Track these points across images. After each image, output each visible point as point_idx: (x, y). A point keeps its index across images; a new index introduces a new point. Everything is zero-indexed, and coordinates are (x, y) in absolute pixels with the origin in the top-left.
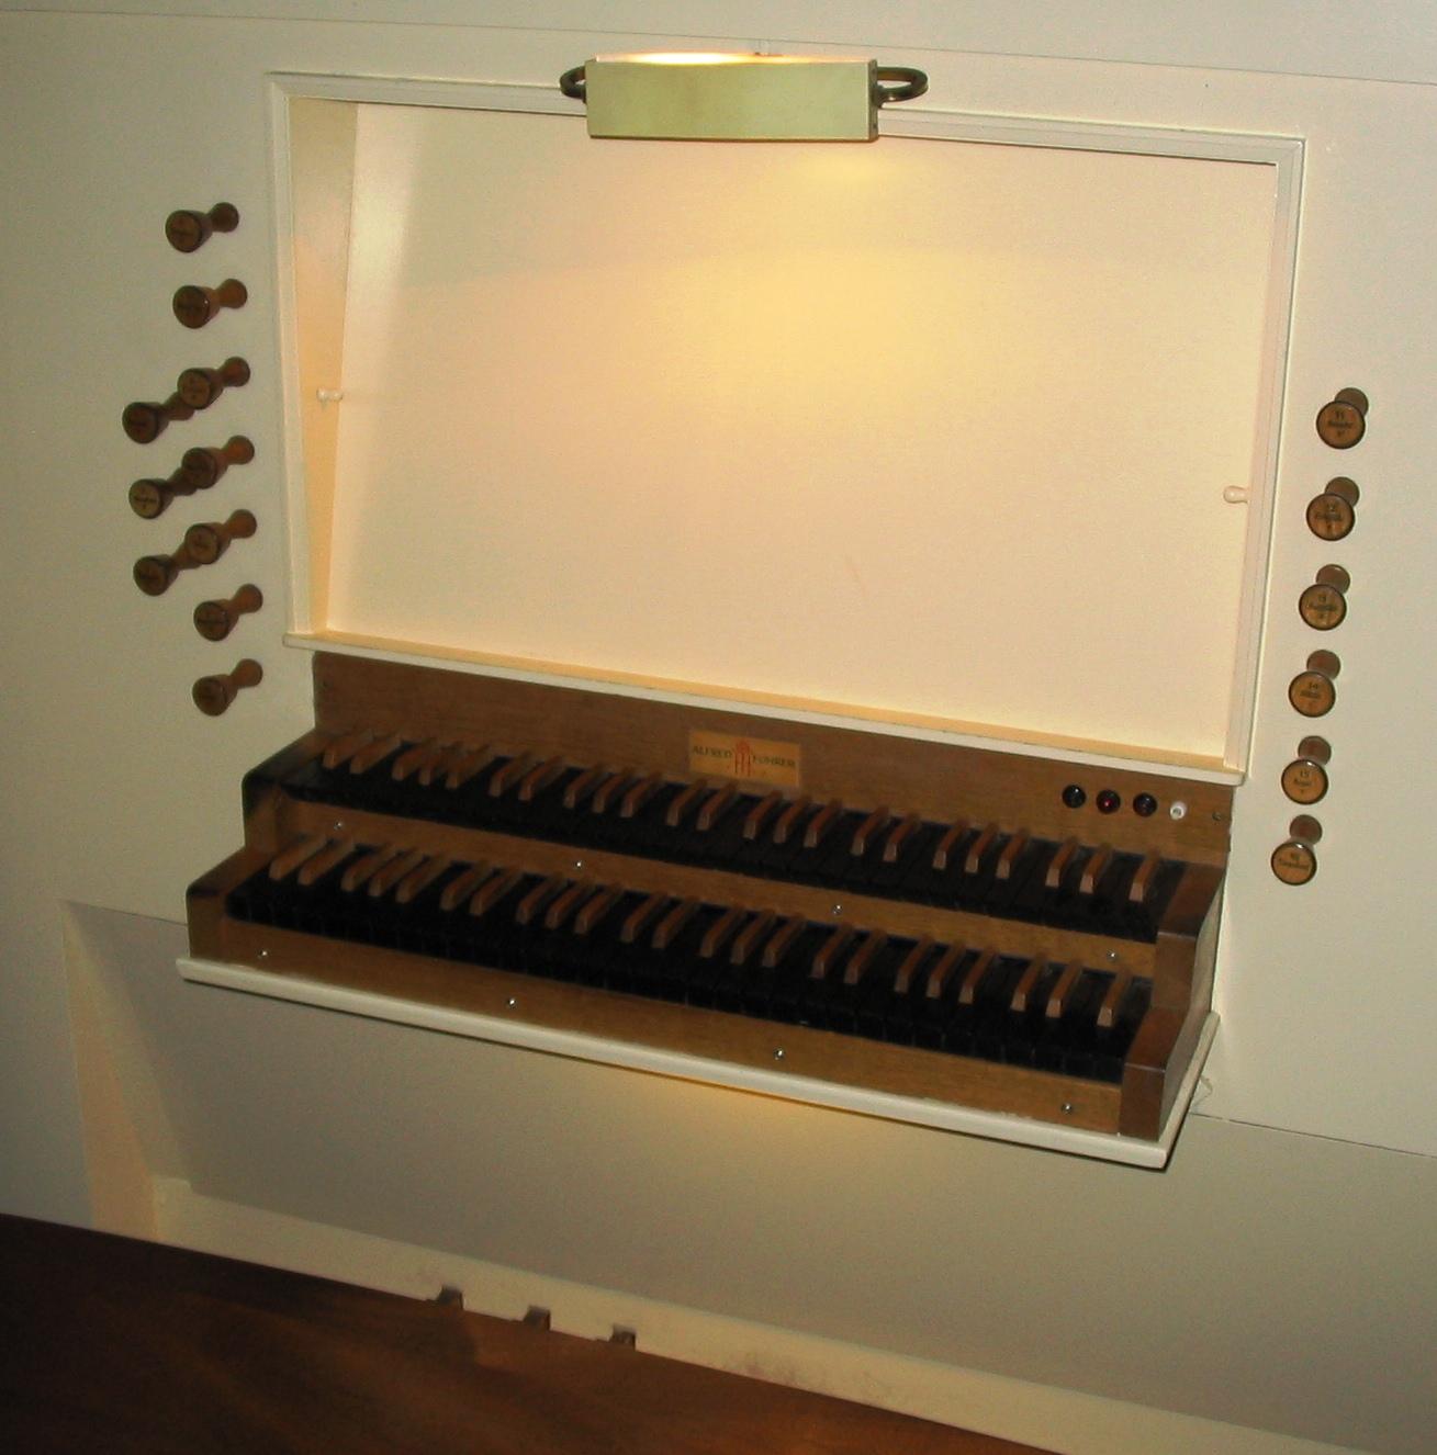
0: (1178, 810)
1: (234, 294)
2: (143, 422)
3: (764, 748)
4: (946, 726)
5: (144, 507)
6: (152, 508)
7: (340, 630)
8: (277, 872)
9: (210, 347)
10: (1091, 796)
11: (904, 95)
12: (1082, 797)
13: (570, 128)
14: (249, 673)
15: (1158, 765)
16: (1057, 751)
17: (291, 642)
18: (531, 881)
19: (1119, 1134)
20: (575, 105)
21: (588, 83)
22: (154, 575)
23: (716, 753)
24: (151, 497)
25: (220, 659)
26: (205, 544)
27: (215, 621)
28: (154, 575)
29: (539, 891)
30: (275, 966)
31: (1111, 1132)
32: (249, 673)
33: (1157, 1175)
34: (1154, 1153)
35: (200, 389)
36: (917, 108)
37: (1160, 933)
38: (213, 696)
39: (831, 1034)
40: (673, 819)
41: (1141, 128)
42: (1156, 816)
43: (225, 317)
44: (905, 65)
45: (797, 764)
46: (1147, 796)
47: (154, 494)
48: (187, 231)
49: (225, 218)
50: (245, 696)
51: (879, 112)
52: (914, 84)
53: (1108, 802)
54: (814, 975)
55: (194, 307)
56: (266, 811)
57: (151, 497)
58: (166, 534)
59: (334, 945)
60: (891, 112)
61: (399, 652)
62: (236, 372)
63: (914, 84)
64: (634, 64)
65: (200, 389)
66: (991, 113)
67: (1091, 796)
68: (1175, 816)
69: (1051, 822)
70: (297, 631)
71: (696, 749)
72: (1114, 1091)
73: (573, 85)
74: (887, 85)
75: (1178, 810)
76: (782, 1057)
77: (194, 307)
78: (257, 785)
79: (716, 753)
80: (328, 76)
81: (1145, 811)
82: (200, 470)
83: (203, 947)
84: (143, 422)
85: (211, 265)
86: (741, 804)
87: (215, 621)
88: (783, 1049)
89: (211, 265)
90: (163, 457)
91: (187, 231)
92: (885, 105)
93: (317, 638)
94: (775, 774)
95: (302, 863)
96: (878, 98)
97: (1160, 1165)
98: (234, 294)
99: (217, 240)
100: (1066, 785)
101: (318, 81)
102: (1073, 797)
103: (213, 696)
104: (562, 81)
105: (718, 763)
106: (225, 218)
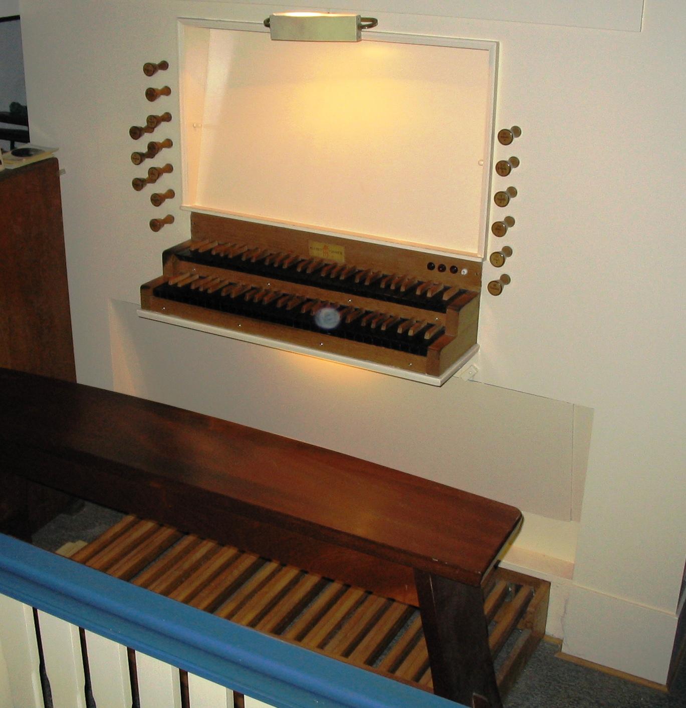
0: (465, 272)
1: (167, 91)
2: (136, 133)
3: (333, 248)
4: (355, 235)
5: (136, 161)
6: (138, 161)
7: (201, 205)
8: (171, 283)
9: (159, 107)
10: (437, 267)
11: (370, 26)
12: (439, 268)
13: (265, 36)
14: (170, 219)
15: (473, 258)
16: (449, 254)
17: (183, 208)
18: (367, 313)
19: (426, 374)
20: (268, 29)
21: (271, 23)
22: (138, 184)
23: (318, 249)
24: (138, 158)
25: (159, 213)
26: (155, 174)
27: (157, 200)
28: (138, 184)
29: (368, 317)
30: (166, 313)
31: (423, 373)
32: (170, 219)
33: (439, 388)
34: (437, 381)
35: (154, 122)
36: (375, 31)
37: (447, 310)
38: (156, 225)
39: (383, 348)
40: (299, 270)
41: (447, 38)
42: (457, 274)
43: (163, 99)
44: (371, 17)
45: (343, 254)
46: (452, 266)
47: (138, 157)
48: (150, 70)
49: (164, 66)
50: (167, 227)
51: (362, 33)
52: (373, 22)
53: (442, 268)
54: (362, 325)
55: (152, 95)
56: (169, 264)
57: (138, 158)
58: (142, 171)
59: (390, 351)
60: (365, 33)
61: (308, 228)
62: (167, 117)
63: (373, 22)
64: (284, 16)
65: (154, 122)
66: (480, 39)
67: (437, 267)
68: (462, 273)
69: (420, 274)
70: (184, 205)
71: (311, 248)
72: (424, 359)
73: (267, 23)
74: (363, 23)
75: (465, 272)
76: (411, 366)
77: (152, 95)
78: (167, 255)
79: (318, 249)
80: (197, 19)
81: (453, 270)
82: (153, 150)
83: (145, 305)
84: (136, 133)
85: (158, 81)
86: (321, 266)
87: (157, 200)
88: (241, 325)
89: (158, 81)
90: (142, 146)
91: (150, 70)
92: (363, 30)
93: (191, 207)
94: (337, 257)
95: (180, 281)
96: (361, 27)
97: (439, 385)
98: (167, 91)
99: (160, 72)
100: (431, 261)
101: (194, 21)
102: (431, 266)
103: (156, 225)
104: (264, 22)
105: (317, 252)
106: (164, 66)
